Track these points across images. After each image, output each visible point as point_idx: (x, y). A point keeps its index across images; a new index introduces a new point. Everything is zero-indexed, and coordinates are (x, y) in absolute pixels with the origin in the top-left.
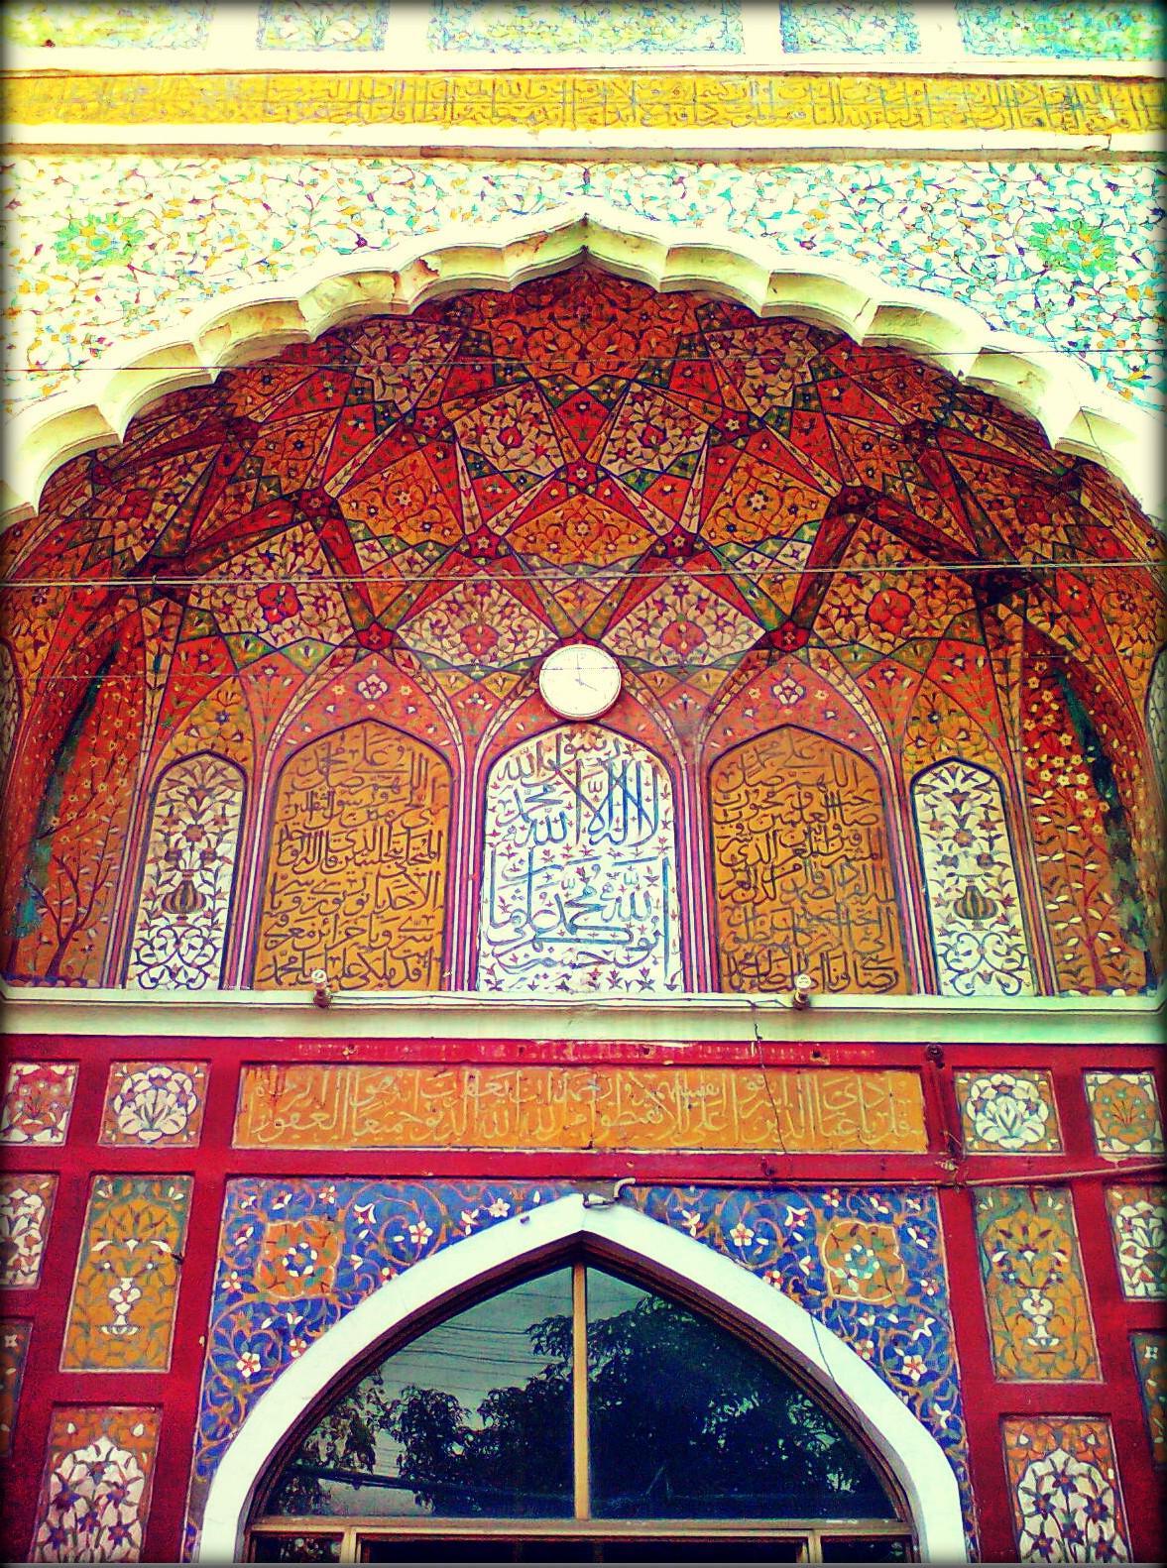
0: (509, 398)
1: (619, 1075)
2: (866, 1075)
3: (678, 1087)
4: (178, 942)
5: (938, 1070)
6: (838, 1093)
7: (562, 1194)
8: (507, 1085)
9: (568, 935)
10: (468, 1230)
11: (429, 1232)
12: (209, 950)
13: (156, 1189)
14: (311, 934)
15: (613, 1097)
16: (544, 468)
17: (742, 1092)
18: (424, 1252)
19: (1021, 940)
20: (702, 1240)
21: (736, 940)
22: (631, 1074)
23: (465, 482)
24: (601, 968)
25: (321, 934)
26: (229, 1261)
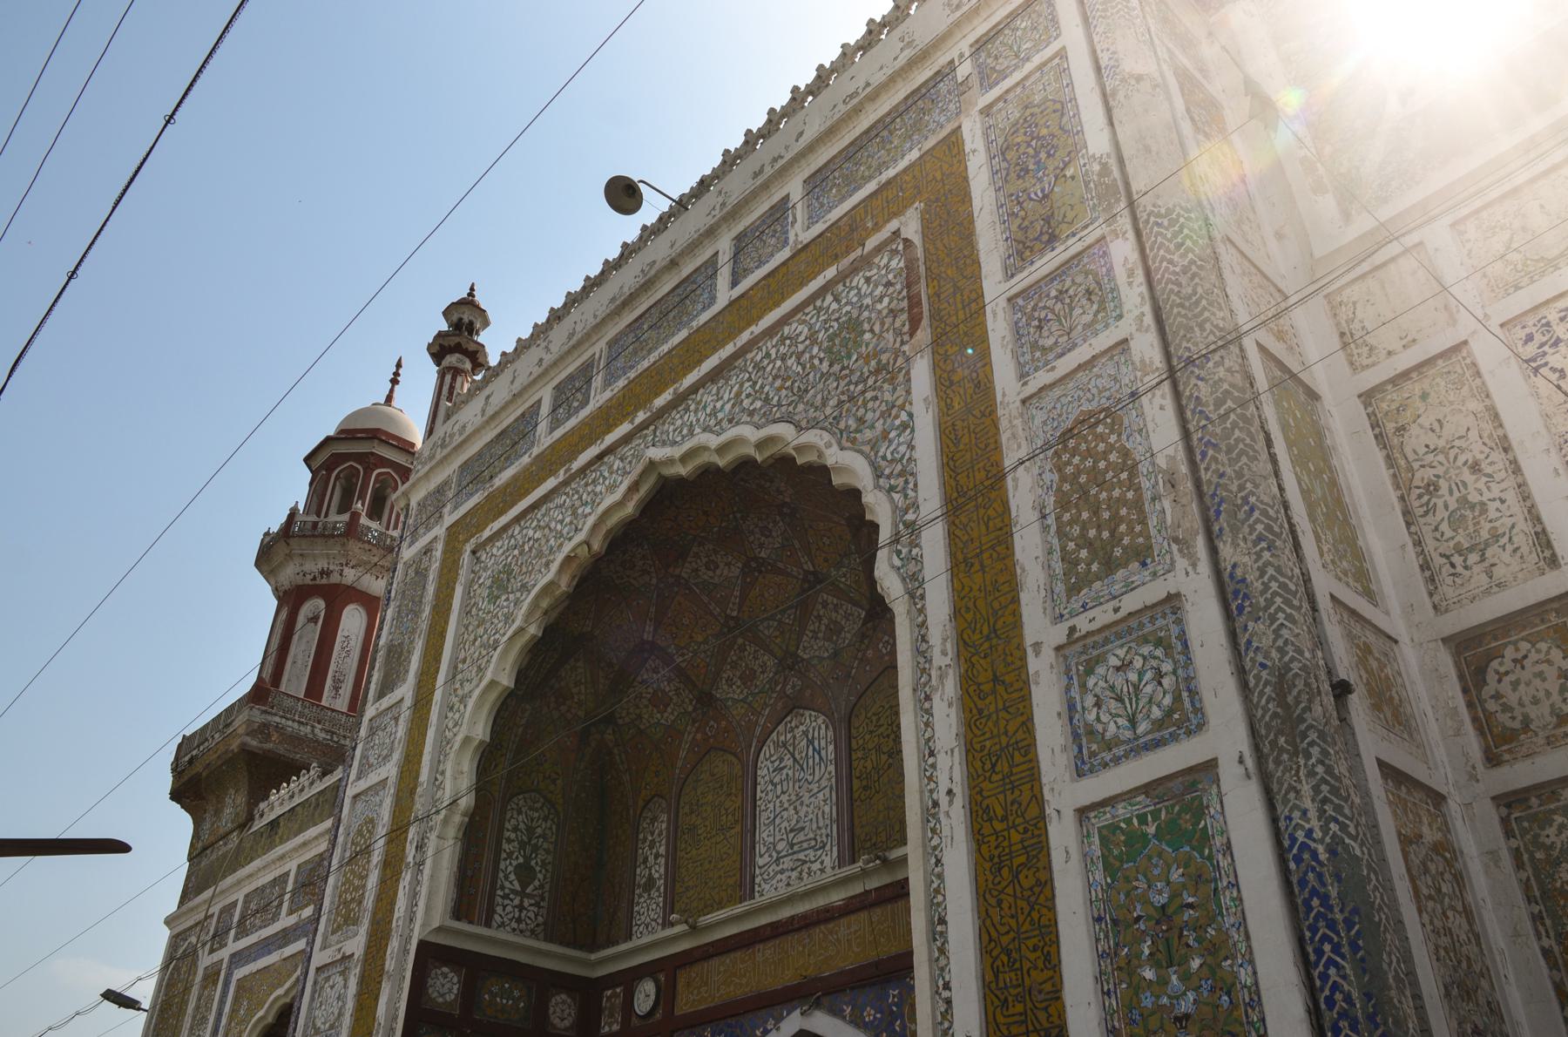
0: (695, 549)
16: (736, 571)
23: (706, 599)
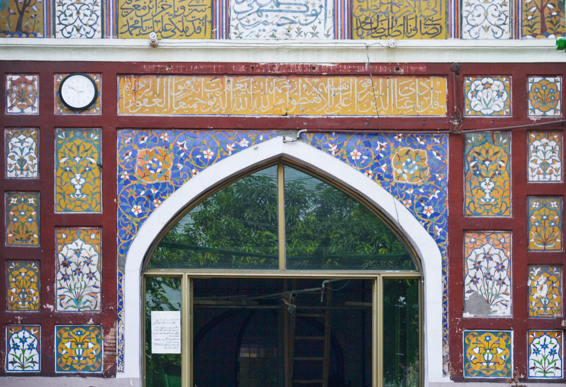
1: (300, 80)
2: (421, 79)
3: (329, 85)
4: (78, 13)
5: (457, 76)
6: (406, 88)
7: (273, 136)
8: (246, 84)
9: (275, 8)
10: (230, 153)
11: (212, 154)
12: (94, 16)
13: (85, 134)
14: (144, 8)
15: (297, 91)
17: (360, 88)
18: (211, 162)
19: (507, 8)
20: (337, 157)
21: (362, 10)
22: (306, 79)
24: (292, 26)
25: (150, 8)
26: (123, 167)
